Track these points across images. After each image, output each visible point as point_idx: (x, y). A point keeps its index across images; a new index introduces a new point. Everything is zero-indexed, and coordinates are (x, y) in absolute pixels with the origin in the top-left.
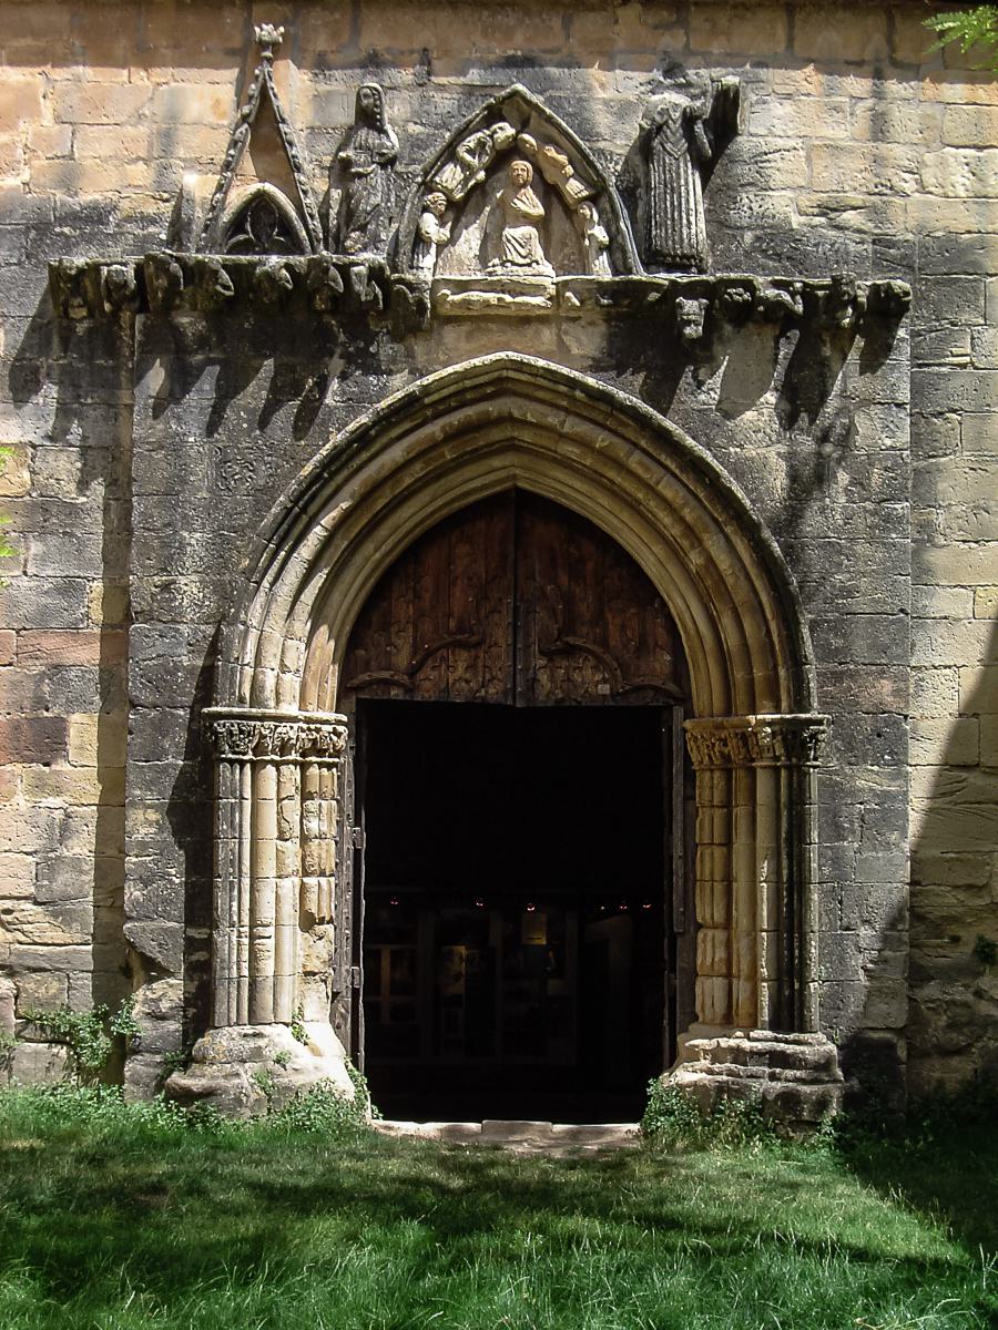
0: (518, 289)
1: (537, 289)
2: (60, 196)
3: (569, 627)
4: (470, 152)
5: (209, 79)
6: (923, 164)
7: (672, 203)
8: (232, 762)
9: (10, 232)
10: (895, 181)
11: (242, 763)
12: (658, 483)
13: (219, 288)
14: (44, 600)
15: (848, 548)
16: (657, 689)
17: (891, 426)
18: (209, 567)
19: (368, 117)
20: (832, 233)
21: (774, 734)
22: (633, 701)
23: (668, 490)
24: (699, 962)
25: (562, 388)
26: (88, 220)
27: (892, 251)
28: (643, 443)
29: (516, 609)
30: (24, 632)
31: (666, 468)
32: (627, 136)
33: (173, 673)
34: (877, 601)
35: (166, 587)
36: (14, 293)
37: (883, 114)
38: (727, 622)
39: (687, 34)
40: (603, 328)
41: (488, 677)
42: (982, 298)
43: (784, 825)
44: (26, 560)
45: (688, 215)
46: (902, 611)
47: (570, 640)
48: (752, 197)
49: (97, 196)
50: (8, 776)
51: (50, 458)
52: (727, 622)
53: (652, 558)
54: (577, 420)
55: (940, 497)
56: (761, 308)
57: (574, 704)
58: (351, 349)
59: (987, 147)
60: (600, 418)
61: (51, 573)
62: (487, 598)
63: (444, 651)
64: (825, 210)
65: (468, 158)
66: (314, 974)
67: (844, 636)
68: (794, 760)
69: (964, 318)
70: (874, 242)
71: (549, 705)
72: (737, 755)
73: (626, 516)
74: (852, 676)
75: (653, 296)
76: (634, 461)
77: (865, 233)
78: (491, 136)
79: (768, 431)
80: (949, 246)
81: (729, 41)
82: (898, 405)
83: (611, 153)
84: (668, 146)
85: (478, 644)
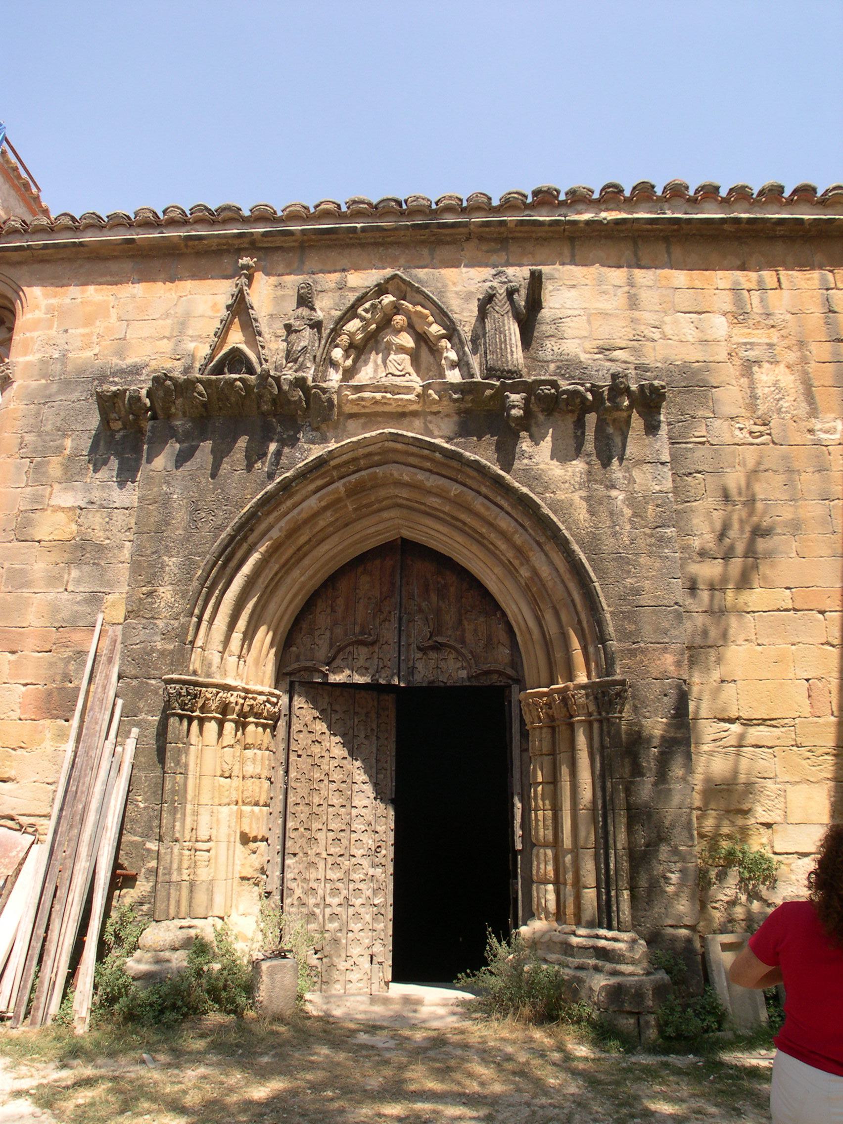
0: (396, 391)
1: (409, 390)
2: (115, 360)
3: (438, 630)
4: (366, 311)
5: (212, 292)
6: (663, 322)
7: (500, 340)
8: (181, 717)
9: (83, 382)
10: (646, 332)
11: (190, 720)
12: (495, 518)
13: (195, 394)
14: (77, 608)
15: (634, 561)
16: (500, 673)
17: (659, 477)
18: (180, 581)
19: (304, 300)
20: (608, 364)
21: (587, 695)
22: (485, 682)
23: (504, 523)
24: (534, 872)
25: (426, 452)
26: (130, 373)
27: (648, 374)
28: (484, 490)
29: (400, 619)
30: (61, 629)
31: (501, 508)
32: (471, 311)
33: (149, 654)
34: (658, 597)
35: (150, 594)
36: (80, 417)
37: (634, 295)
38: (549, 617)
39: (507, 254)
40: (456, 418)
41: (381, 665)
42: (710, 401)
43: (598, 765)
44: (68, 582)
45: (511, 347)
46: (676, 603)
47: (440, 639)
48: (553, 343)
49: (137, 360)
50: (41, 728)
51: (90, 516)
52: (549, 617)
53: (494, 577)
54: (437, 477)
55: (694, 528)
56: (565, 396)
57: (442, 684)
58: (285, 436)
59: (704, 312)
60: (452, 474)
61: (82, 589)
62: (381, 611)
63: (350, 648)
64: (602, 350)
65: (363, 313)
66: (249, 879)
67: (635, 623)
68: (604, 714)
69: (700, 413)
70: (636, 368)
71: (424, 685)
72: (559, 713)
73: (475, 548)
74: (643, 651)
75: (488, 392)
76: (478, 504)
77: (629, 363)
78: (380, 302)
79: (572, 482)
80: (685, 370)
81: (533, 257)
82: (662, 464)
83: (460, 321)
84: (497, 308)
85: (373, 643)
